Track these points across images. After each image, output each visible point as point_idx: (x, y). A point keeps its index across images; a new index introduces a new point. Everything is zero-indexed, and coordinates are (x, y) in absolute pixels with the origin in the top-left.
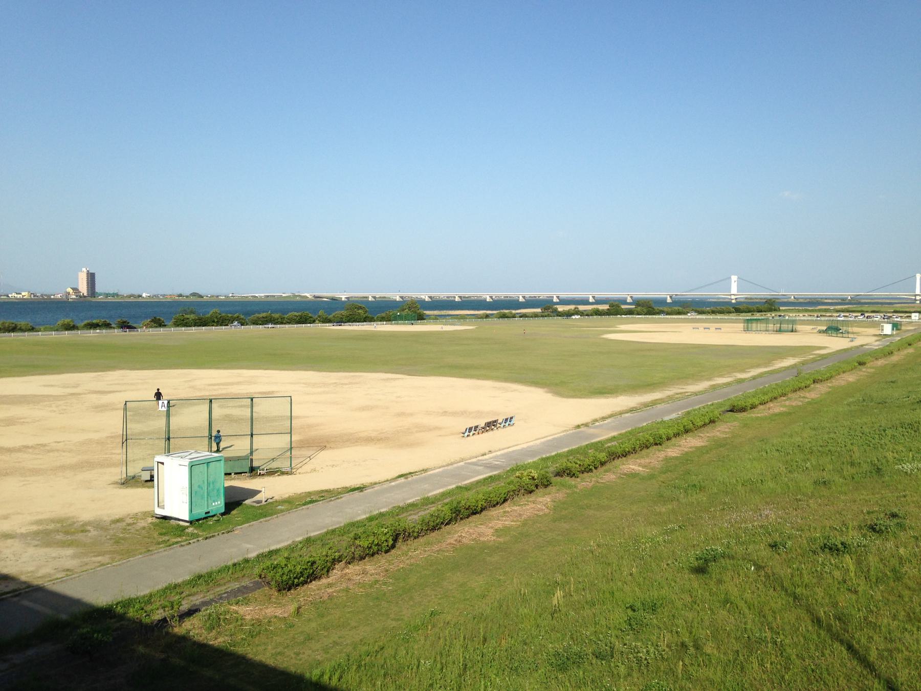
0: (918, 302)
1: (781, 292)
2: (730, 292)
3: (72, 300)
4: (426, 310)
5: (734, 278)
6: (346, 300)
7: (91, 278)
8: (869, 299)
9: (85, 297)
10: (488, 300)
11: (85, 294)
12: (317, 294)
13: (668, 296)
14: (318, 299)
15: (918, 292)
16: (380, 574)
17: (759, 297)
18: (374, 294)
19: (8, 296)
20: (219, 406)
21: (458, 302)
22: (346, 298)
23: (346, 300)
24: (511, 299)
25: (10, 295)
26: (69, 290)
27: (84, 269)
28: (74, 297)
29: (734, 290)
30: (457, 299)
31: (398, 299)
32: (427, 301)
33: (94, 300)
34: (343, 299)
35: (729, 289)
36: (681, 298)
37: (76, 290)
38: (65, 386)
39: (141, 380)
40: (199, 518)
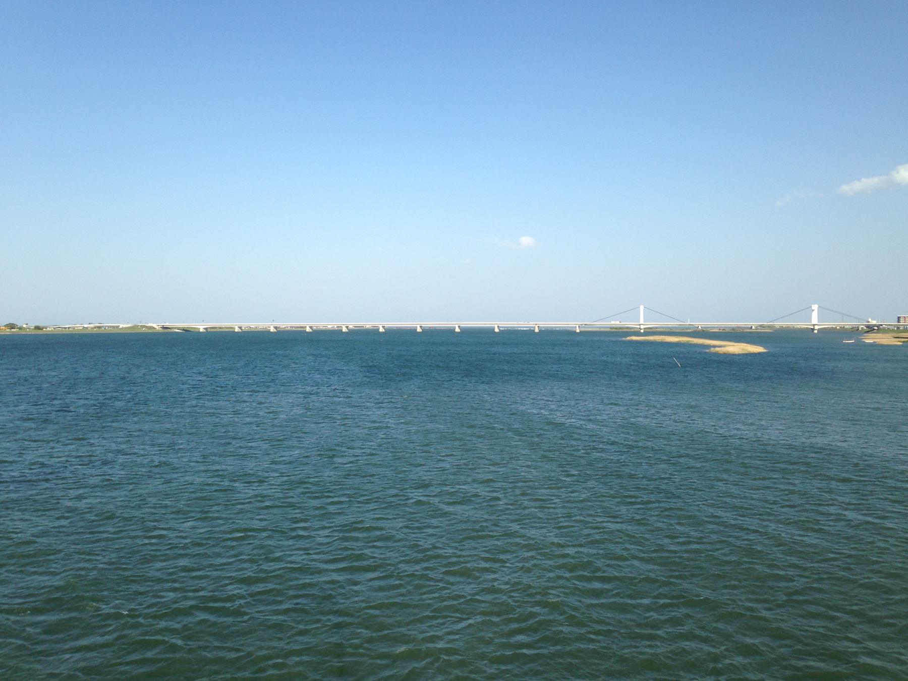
0: (816, 331)
5: (642, 307)
6: (205, 331)
12: (167, 324)
13: (577, 326)
14: (166, 331)
15: (642, 322)
23: (205, 331)
29: (642, 322)
34: (201, 330)
35: (810, 320)
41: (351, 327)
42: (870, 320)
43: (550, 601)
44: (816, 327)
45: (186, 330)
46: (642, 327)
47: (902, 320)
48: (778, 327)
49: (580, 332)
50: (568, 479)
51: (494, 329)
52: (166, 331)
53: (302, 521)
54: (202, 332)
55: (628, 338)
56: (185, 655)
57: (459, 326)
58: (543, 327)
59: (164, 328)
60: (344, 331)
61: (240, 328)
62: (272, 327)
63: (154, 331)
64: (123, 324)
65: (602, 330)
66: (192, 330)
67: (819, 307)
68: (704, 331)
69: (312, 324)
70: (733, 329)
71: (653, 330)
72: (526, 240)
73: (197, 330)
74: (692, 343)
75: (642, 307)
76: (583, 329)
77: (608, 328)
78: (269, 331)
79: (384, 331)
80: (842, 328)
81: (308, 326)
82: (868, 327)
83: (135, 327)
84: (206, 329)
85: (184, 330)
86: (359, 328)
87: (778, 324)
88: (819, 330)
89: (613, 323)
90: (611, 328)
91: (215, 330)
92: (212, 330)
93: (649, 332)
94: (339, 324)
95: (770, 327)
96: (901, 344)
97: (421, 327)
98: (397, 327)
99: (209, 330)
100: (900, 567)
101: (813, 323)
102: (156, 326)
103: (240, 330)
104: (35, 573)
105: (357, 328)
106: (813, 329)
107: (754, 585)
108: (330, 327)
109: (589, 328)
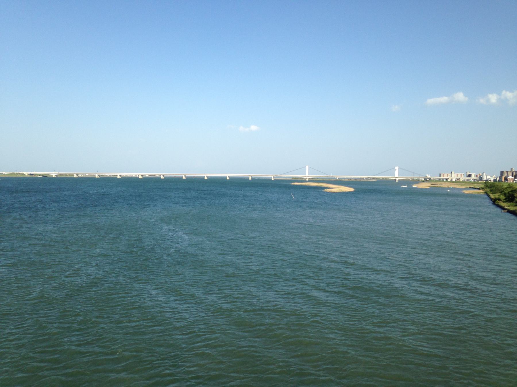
0: (397, 181)
1: (331, 175)
2: (394, 176)
4: (292, 183)
5: (307, 167)
6: (56, 177)
8: (281, 178)
12: (32, 173)
13: (272, 177)
14: (32, 176)
15: (307, 175)
16: (157, 222)
17: (295, 177)
22: (56, 175)
29: (396, 175)
30: (162, 177)
32: (54, 177)
34: (54, 176)
35: (394, 175)
40: (510, 215)
41: (80, 175)
42: (427, 175)
44: (397, 179)
45: (44, 176)
46: (307, 178)
47: (442, 175)
48: (381, 178)
49: (274, 180)
51: (226, 177)
52: (32, 176)
53: (183, 289)
54: (55, 177)
55: (293, 184)
56: (437, 378)
57: (207, 176)
58: (254, 177)
59: (30, 174)
61: (77, 175)
63: (24, 176)
64: (6, 172)
65: (287, 179)
66: (49, 176)
67: (399, 168)
68: (340, 180)
69: (121, 173)
70: (355, 179)
71: (314, 179)
72: (254, 128)
73: (51, 176)
74: (323, 186)
75: (307, 167)
76: (275, 179)
77: (290, 178)
78: (74, 178)
79: (164, 178)
80: (413, 179)
81: (118, 175)
82: (425, 179)
83: (13, 174)
86: (152, 176)
87: (381, 177)
88: (398, 180)
89: (34, 172)
90: (292, 178)
91: (63, 176)
92: (61, 176)
93: (312, 180)
95: (373, 178)
96: (429, 188)
97: (185, 176)
98: (175, 176)
99: (58, 176)
101: (396, 177)
102: (26, 174)
103: (77, 177)
104: (197, 325)
105: (151, 176)
106: (396, 180)
108: (134, 175)
109: (278, 178)
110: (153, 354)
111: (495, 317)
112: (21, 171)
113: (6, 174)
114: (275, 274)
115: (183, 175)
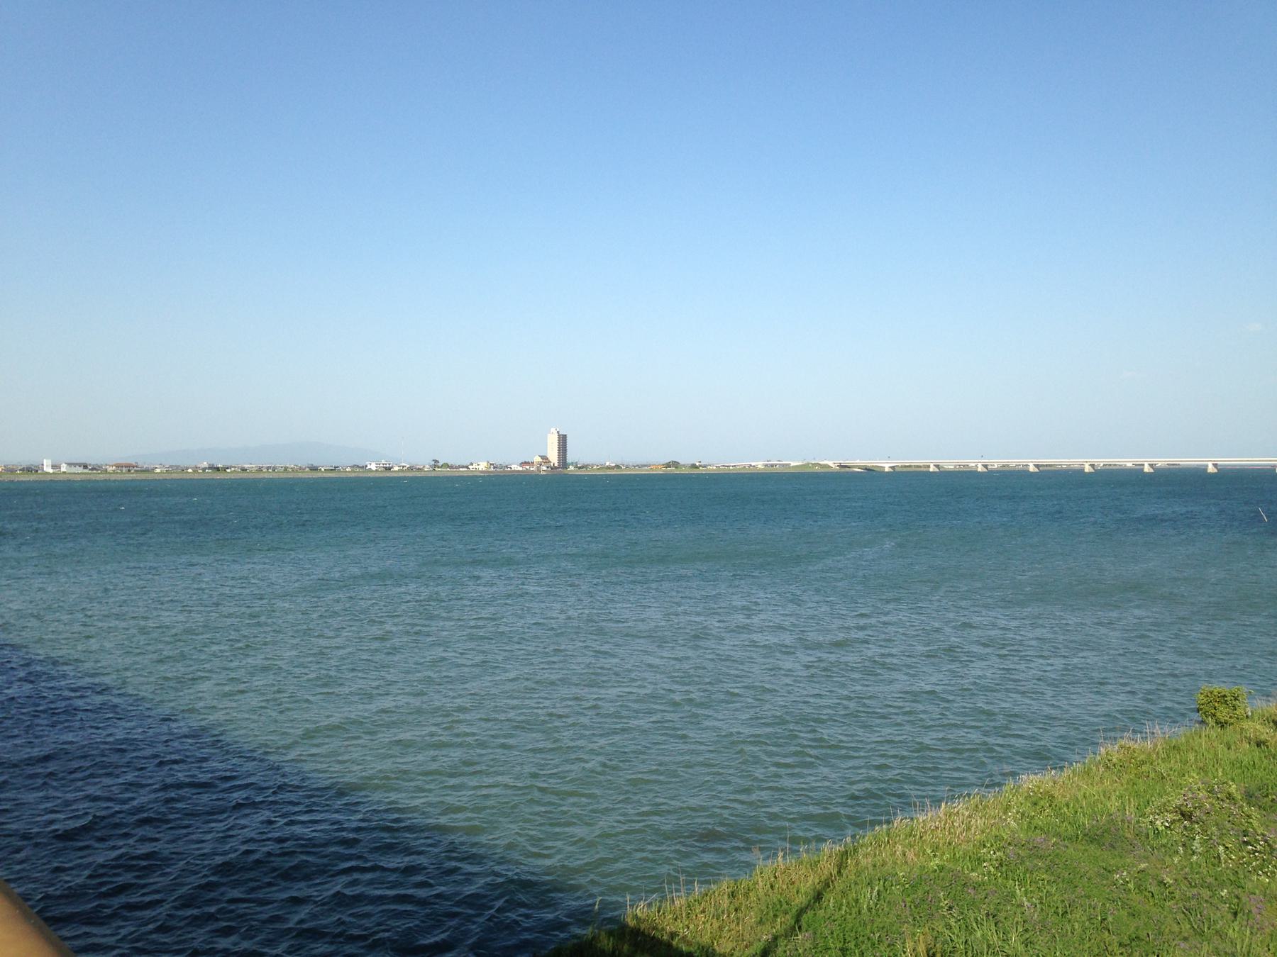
3: (544, 473)
6: (891, 470)
7: (563, 440)
9: (556, 468)
10: (1086, 470)
11: (556, 465)
14: (843, 470)
18: (1093, 460)
19: (467, 467)
20: (620, 907)
21: (1090, 473)
23: (891, 470)
24: (1115, 467)
25: (470, 467)
26: (537, 459)
27: (553, 430)
28: (545, 468)
31: (980, 469)
33: (565, 471)
36: (1235, 465)
37: (544, 458)
38: (543, 759)
39: (1017, 722)
43: (315, 952)
50: (37, 741)
52: (843, 470)
59: (841, 466)
60: (1086, 470)
62: (1031, 465)
69: (938, 461)
73: (882, 470)
78: (884, 472)
81: (932, 465)
83: (806, 465)
84: (893, 467)
85: (866, 469)
89: (858, 461)
92: (905, 469)
94: (1139, 460)
99: (897, 469)
100: (148, 924)
102: (832, 464)
103: (985, 470)
105: (1172, 467)
107: (530, 909)
110: (475, 815)
111: (468, 766)
112: (245, 464)
113: (797, 466)
114: (932, 692)
115: (1086, 463)
